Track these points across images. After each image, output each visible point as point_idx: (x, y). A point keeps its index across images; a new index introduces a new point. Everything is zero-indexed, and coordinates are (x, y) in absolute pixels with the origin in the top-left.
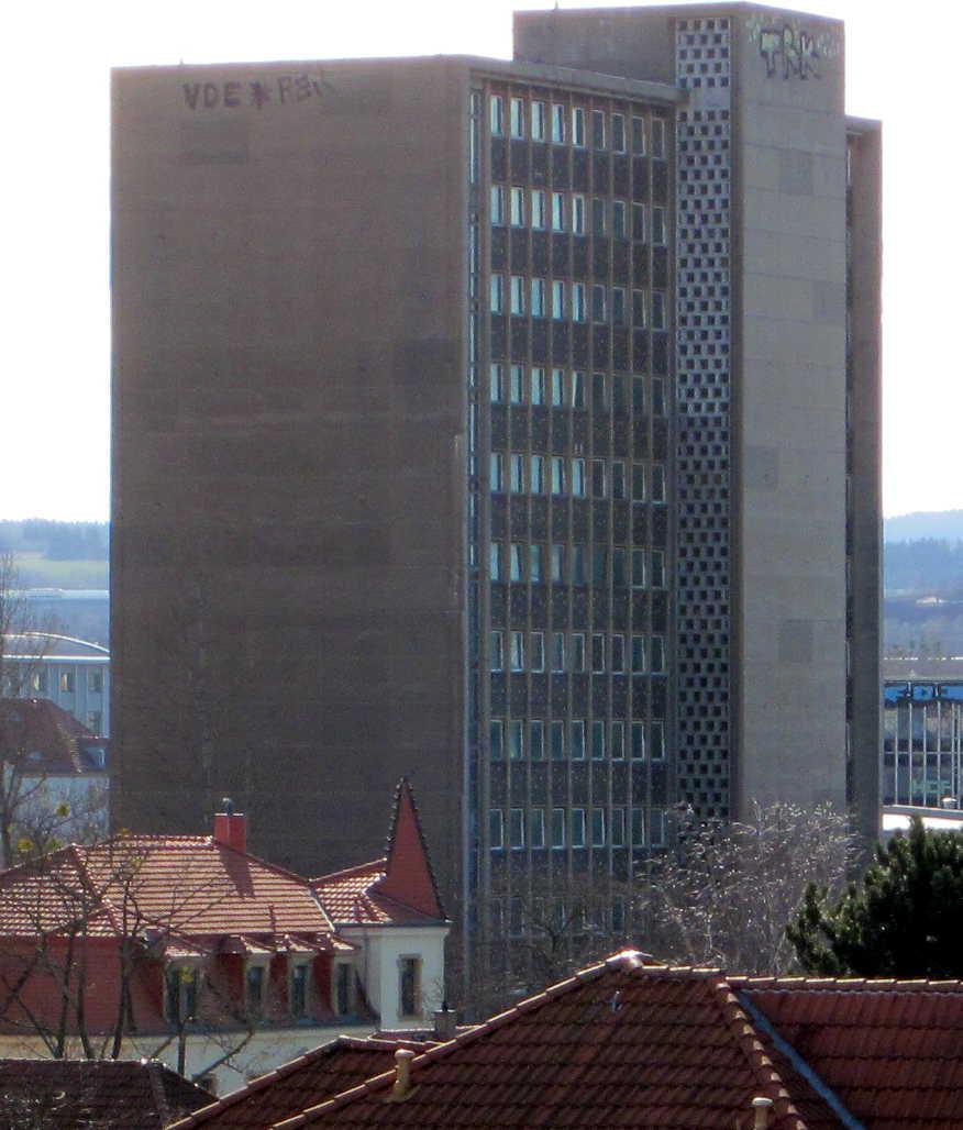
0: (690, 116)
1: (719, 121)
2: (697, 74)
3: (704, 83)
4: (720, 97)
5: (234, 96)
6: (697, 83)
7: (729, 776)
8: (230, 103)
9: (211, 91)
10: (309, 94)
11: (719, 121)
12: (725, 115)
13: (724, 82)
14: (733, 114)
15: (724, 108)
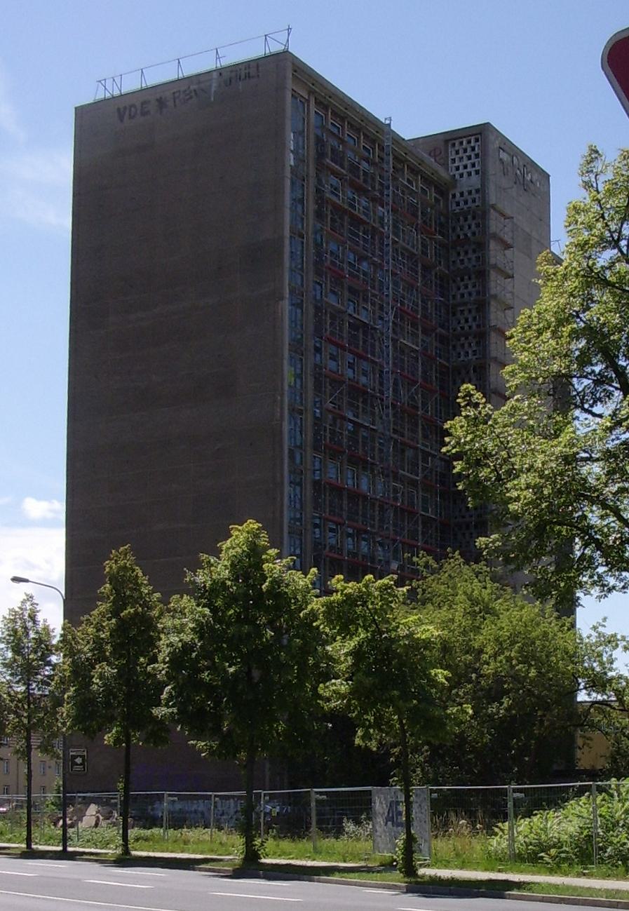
0: (458, 195)
1: (474, 195)
2: (461, 170)
3: (465, 175)
4: (475, 180)
5: (146, 110)
6: (461, 175)
7: (481, 322)
8: (144, 114)
9: (133, 109)
10: (191, 98)
11: (474, 195)
12: (477, 191)
13: (477, 172)
14: (482, 191)
15: (477, 188)
